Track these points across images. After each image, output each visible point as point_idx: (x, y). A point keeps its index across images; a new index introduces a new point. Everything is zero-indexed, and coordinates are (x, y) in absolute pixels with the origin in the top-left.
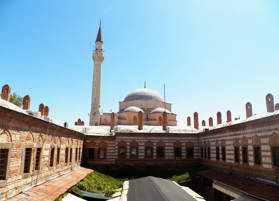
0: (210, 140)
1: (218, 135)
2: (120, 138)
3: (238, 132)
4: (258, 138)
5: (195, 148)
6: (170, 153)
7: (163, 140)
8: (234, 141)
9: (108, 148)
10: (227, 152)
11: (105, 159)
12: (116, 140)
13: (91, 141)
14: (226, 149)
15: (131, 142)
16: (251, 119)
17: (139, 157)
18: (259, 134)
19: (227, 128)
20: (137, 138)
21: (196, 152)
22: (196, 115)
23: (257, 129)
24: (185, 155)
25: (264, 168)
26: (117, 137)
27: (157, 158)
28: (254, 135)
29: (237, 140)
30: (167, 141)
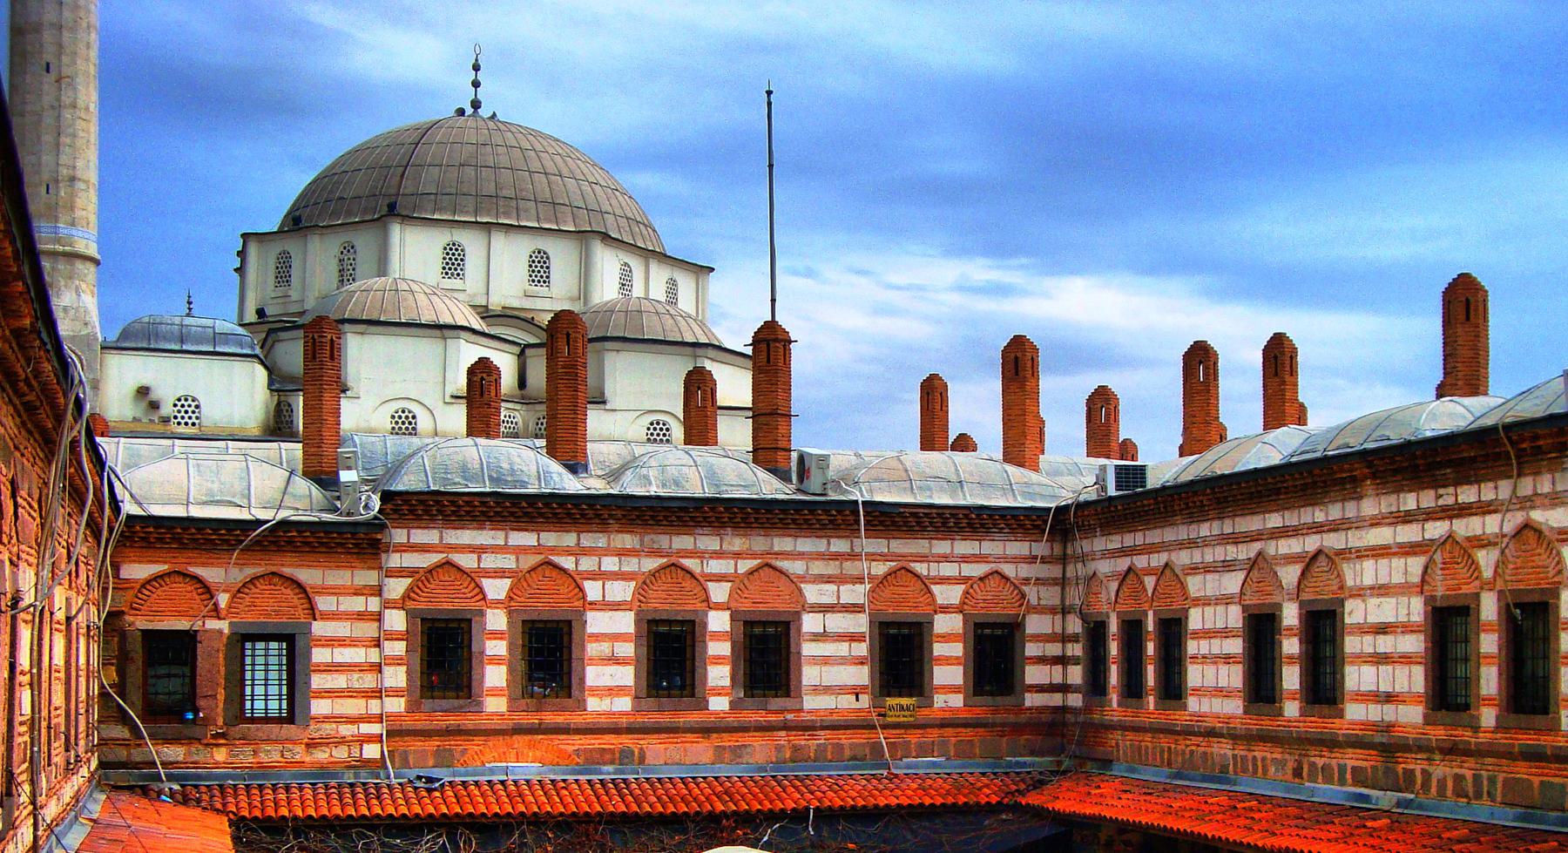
0: (1183, 558)
1: (1274, 520)
2: (421, 536)
3: (1467, 495)
5: (1036, 624)
8: (1431, 561)
9: (315, 624)
11: (290, 719)
12: (395, 560)
13: (164, 567)
14: (1347, 620)
17: (593, 704)
19: (1370, 465)
20: (569, 539)
21: (1042, 660)
24: (936, 669)
26: (399, 536)
29: (1460, 551)
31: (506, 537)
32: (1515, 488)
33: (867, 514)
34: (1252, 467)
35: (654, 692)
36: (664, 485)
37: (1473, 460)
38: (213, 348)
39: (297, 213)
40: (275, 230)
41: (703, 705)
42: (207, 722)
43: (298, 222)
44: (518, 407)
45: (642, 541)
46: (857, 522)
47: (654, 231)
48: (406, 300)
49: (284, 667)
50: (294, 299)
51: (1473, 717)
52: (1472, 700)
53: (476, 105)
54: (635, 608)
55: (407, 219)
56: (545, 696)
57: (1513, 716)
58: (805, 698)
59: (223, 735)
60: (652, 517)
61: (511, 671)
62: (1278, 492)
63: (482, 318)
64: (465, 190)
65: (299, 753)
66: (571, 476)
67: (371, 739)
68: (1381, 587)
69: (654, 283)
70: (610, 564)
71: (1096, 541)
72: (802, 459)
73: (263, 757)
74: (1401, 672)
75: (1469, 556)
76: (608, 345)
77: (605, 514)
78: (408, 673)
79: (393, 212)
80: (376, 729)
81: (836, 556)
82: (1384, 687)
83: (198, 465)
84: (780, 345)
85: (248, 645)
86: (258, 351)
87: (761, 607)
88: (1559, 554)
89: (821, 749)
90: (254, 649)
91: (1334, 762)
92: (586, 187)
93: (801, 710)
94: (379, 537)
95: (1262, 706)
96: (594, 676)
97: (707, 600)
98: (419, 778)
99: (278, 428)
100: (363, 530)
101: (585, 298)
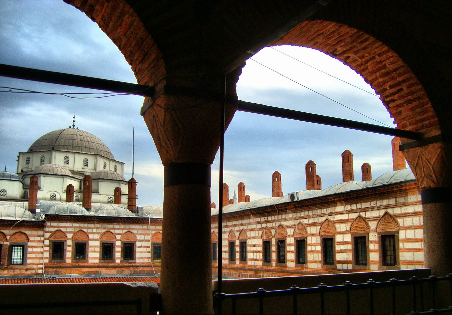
1: (234, 223)
2: (53, 224)
3: (270, 218)
4: (303, 227)
6: (145, 252)
10: (249, 249)
11: (22, 264)
12: (47, 229)
14: (248, 244)
16: (369, 184)
18: (305, 221)
19: (251, 212)
20: (86, 225)
23: (303, 214)
26: (48, 224)
27: (121, 261)
28: (297, 222)
29: (268, 230)
31: (34, 238)
32: (278, 217)
33: (151, 220)
34: (229, 212)
35: (104, 259)
36: (107, 214)
37: (270, 211)
38: (10, 178)
39: (32, 148)
40: (26, 152)
41: (114, 261)
42: (3, 264)
43: (32, 151)
44: (79, 193)
45: (102, 226)
46: (149, 222)
47: (112, 154)
48: (55, 169)
49: (21, 252)
50: (30, 167)
51: (271, 264)
52: (271, 260)
53: (74, 126)
54: (100, 240)
55: (57, 151)
56: (79, 259)
57: (278, 264)
58: (137, 260)
59: (6, 268)
60: (104, 221)
61: (72, 254)
62: (234, 217)
63: (72, 173)
64: (70, 145)
65: (24, 272)
66: (87, 211)
67: (40, 268)
68: (254, 237)
69: (111, 167)
70: (95, 231)
71: (251, 219)
72: (137, 208)
73: (16, 273)
74: (258, 254)
75: (395, 220)
76: (100, 180)
77: (94, 220)
78: (49, 254)
79: (53, 149)
80: (41, 266)
81: (144, 229)
82: (255, 258)
83: (4, 207)
84: (134, 183)
85: (13, 247)
86: (21, 180)
87: (127, 240)
88: (286, 231)
89: (140, 271)
90: (15, 248)
91: (246, 274)
92: (97, 145)
93: (136, 263)
94: (44, 224)
95: (243, 262)
96: (91, 255)
97: (116, 239)
98: (51, 277)
99: (24, 198)
100: (41, 222)
101: (96, 170)
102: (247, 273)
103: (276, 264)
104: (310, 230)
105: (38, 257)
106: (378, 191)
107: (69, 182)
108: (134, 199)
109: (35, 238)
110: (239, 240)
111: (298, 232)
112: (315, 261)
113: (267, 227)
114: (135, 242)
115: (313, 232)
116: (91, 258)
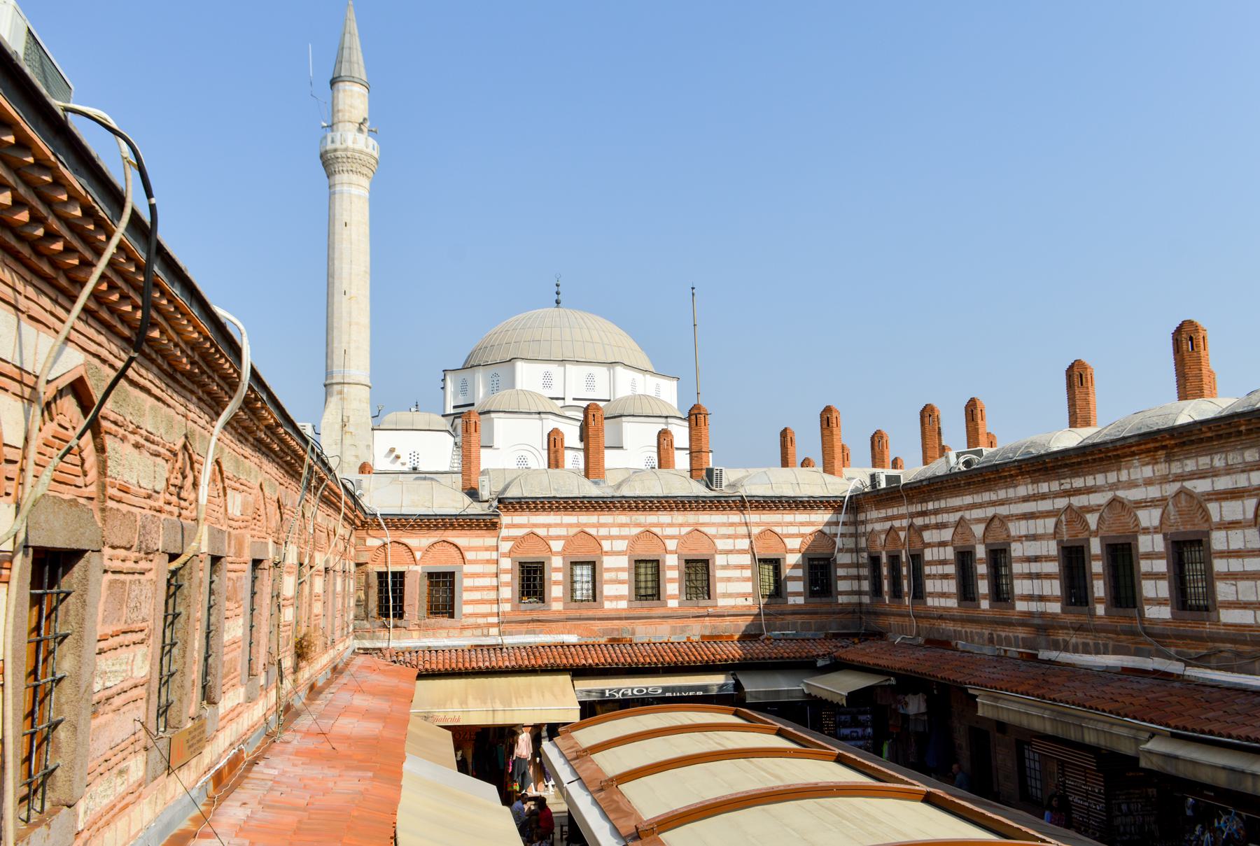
1: (968, 500)
3: (1078, 483)
6: (738, 580)
7: (703, 524)
14: (1013, 554)
15: (569, 540)
18: (1201, 486)
22: (827, 419)
23: (1190, 465)
25: (1225, 625)
28: (1172, 488)
29: (1077, 515)
30: (723, 530)
57: (1114, 609)
70: (615, 531)
81: (732, 524)
87: (694, 552)
102: (1016, 634)
103: (1106, 610)
104: (1221, 511)
105: (486, 597)
106: (1255, 423)
107: (551, 423)
108: (703, 454)
109: (478, 553)
110: (987, 546)
111: (1178, 517)
112: (1245, 604)
113: (1070, 506)
114: (713, 555)
115: (1229, 517)
116: (610, 597)
